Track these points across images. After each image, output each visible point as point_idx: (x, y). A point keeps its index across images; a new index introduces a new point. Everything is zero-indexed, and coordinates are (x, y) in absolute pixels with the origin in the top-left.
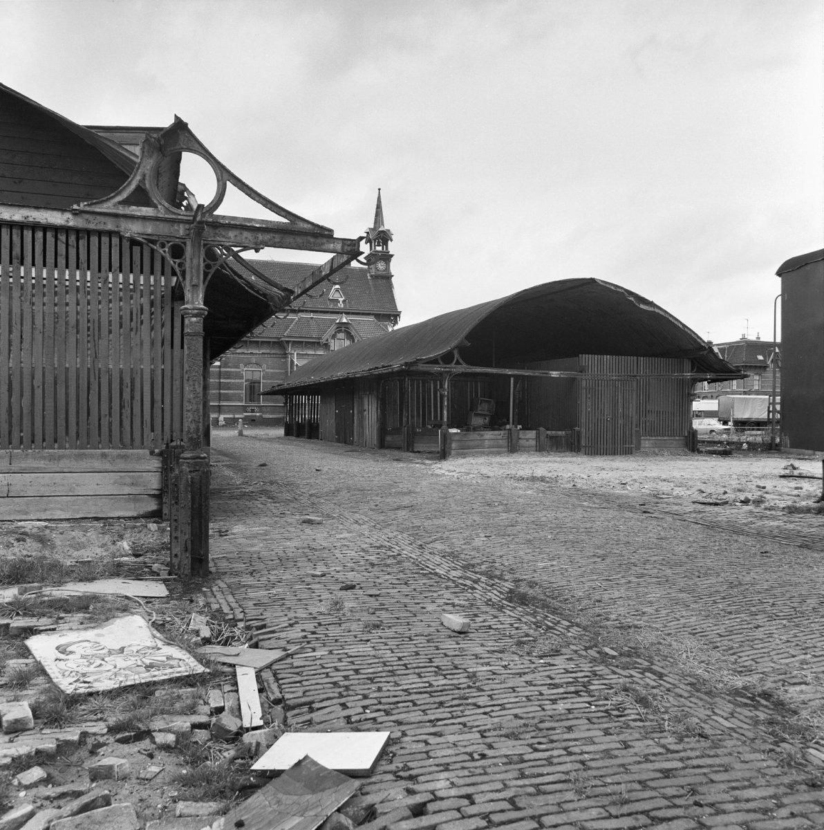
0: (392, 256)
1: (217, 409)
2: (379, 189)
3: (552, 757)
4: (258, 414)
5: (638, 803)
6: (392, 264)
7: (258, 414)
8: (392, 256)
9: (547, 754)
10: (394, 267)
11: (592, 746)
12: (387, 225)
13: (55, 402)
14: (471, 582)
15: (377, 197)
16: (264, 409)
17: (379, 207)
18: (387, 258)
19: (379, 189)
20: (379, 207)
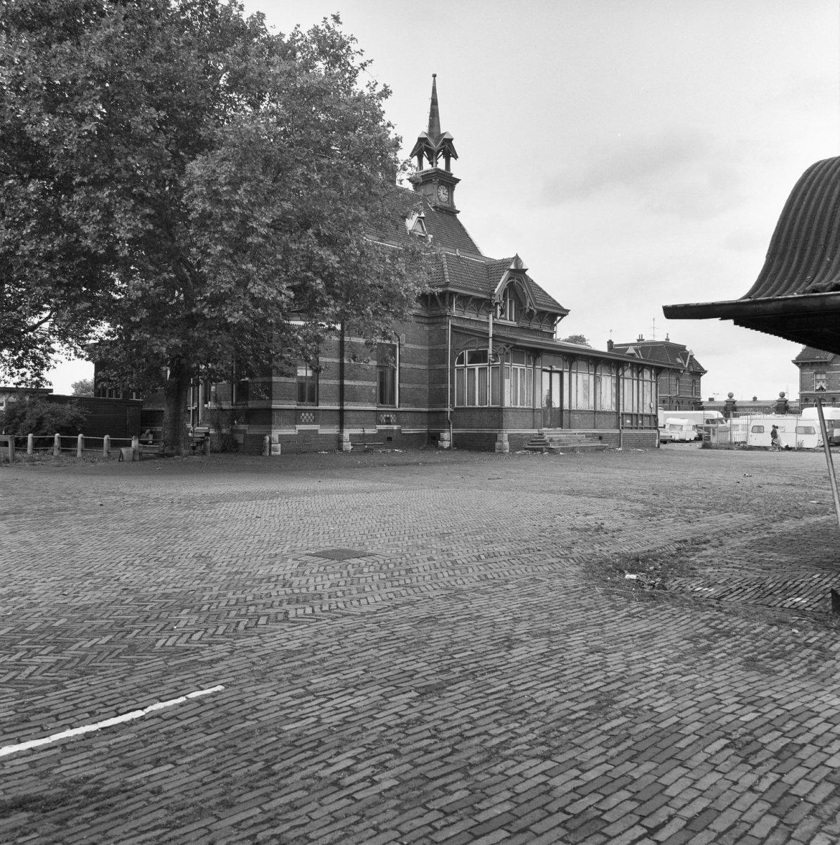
0: (457, 181)
1: (337, 417)
2: (434, 76)
3: (119, 708)
4: (395, 427)
5: (762, 723)
6: (455, 193)
7: (395, 427)
8: (457, 181)
9: (114, 708)
10: (460, 198)
11: (375, 722)
12: (445, 127)
13: (10, 774)
14: (310, 752)
15: (430, 96)
16: (403, 418)
17: (434, 102)
18: (449, 182)
19: (434, 76)
20: (434, 102)
